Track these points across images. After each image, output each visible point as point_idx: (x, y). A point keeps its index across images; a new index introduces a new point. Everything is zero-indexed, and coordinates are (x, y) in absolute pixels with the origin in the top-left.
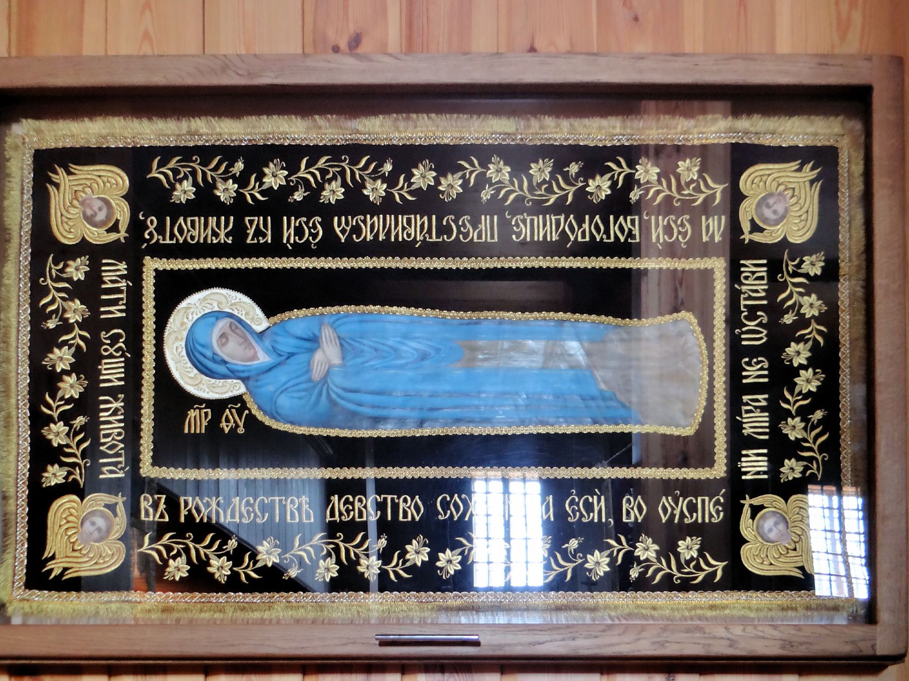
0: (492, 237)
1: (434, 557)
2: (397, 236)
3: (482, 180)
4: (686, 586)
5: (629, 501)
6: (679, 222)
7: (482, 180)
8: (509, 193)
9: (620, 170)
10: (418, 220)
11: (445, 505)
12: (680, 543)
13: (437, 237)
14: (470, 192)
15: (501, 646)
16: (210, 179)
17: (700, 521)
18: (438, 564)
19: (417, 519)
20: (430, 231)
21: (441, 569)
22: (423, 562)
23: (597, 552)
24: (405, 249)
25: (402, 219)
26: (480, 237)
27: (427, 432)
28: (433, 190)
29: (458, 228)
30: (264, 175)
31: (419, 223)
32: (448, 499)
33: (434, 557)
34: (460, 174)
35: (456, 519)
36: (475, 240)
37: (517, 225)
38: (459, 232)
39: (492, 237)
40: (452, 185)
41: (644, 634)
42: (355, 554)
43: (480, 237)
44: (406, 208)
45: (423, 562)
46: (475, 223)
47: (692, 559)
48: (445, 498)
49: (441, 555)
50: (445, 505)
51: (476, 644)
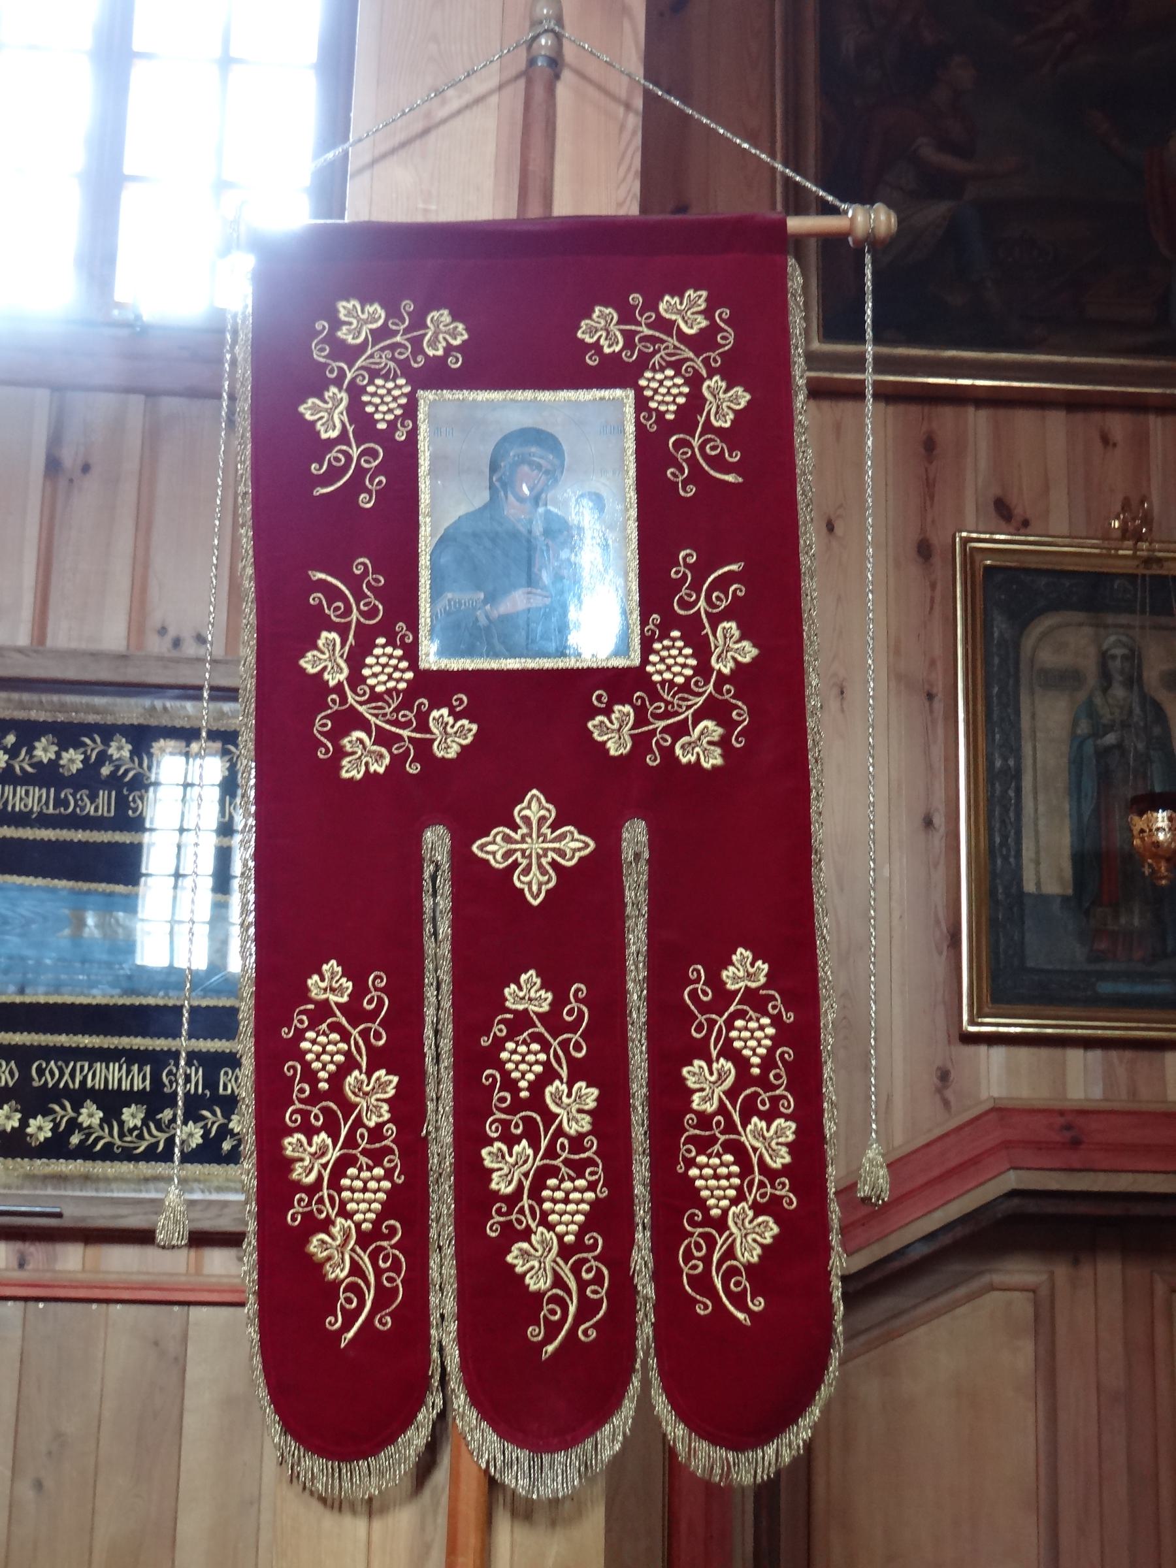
0: (109, 811)
1: (24, 1123)
2: (14, 806)
3: (103, 757)
4: (128, 1155)
5: (226, 1073)
6: (78, 796)
7: (103, 757)
8: (126, 772)
9: (94, 746)
10: (35, 792)
11: (41, 1072)
12: (125, 1110)
13: (54, 808)
14: (91, 767)
15: (84, 1219)
16: (136, 760)
17: (192, 1091)
18: (29, 1130)
19: (11, 1084)
20: (47, 803)
21: (31, 1136)
22: (13, 1128)
23: (39, 1117)
24: (22, 819)
25: (21, 791)
26: (96, 809)
27: (59, 999)
28: (54, 764)
29: (76, 801)
30: (34, 748)
31: (37, 795)
32: (44, 1065)
33: (24, 1123)
34: (82, 750)
35: (50, 1085)
36: (92, 813)
37: (134, 801)
38: (76, 805)
39: (109, 811)
40: (73, 760)
41: (226, 1211)
42: (103, 1129)
43: (96, 809)
44: (26, 780)
45: (13, 1128)
46: (93, 798)
47: (135, 1128)
48: (40, 1065)
49: (32, 1121)
50: (41, 1072)
51: (59, 1215)
